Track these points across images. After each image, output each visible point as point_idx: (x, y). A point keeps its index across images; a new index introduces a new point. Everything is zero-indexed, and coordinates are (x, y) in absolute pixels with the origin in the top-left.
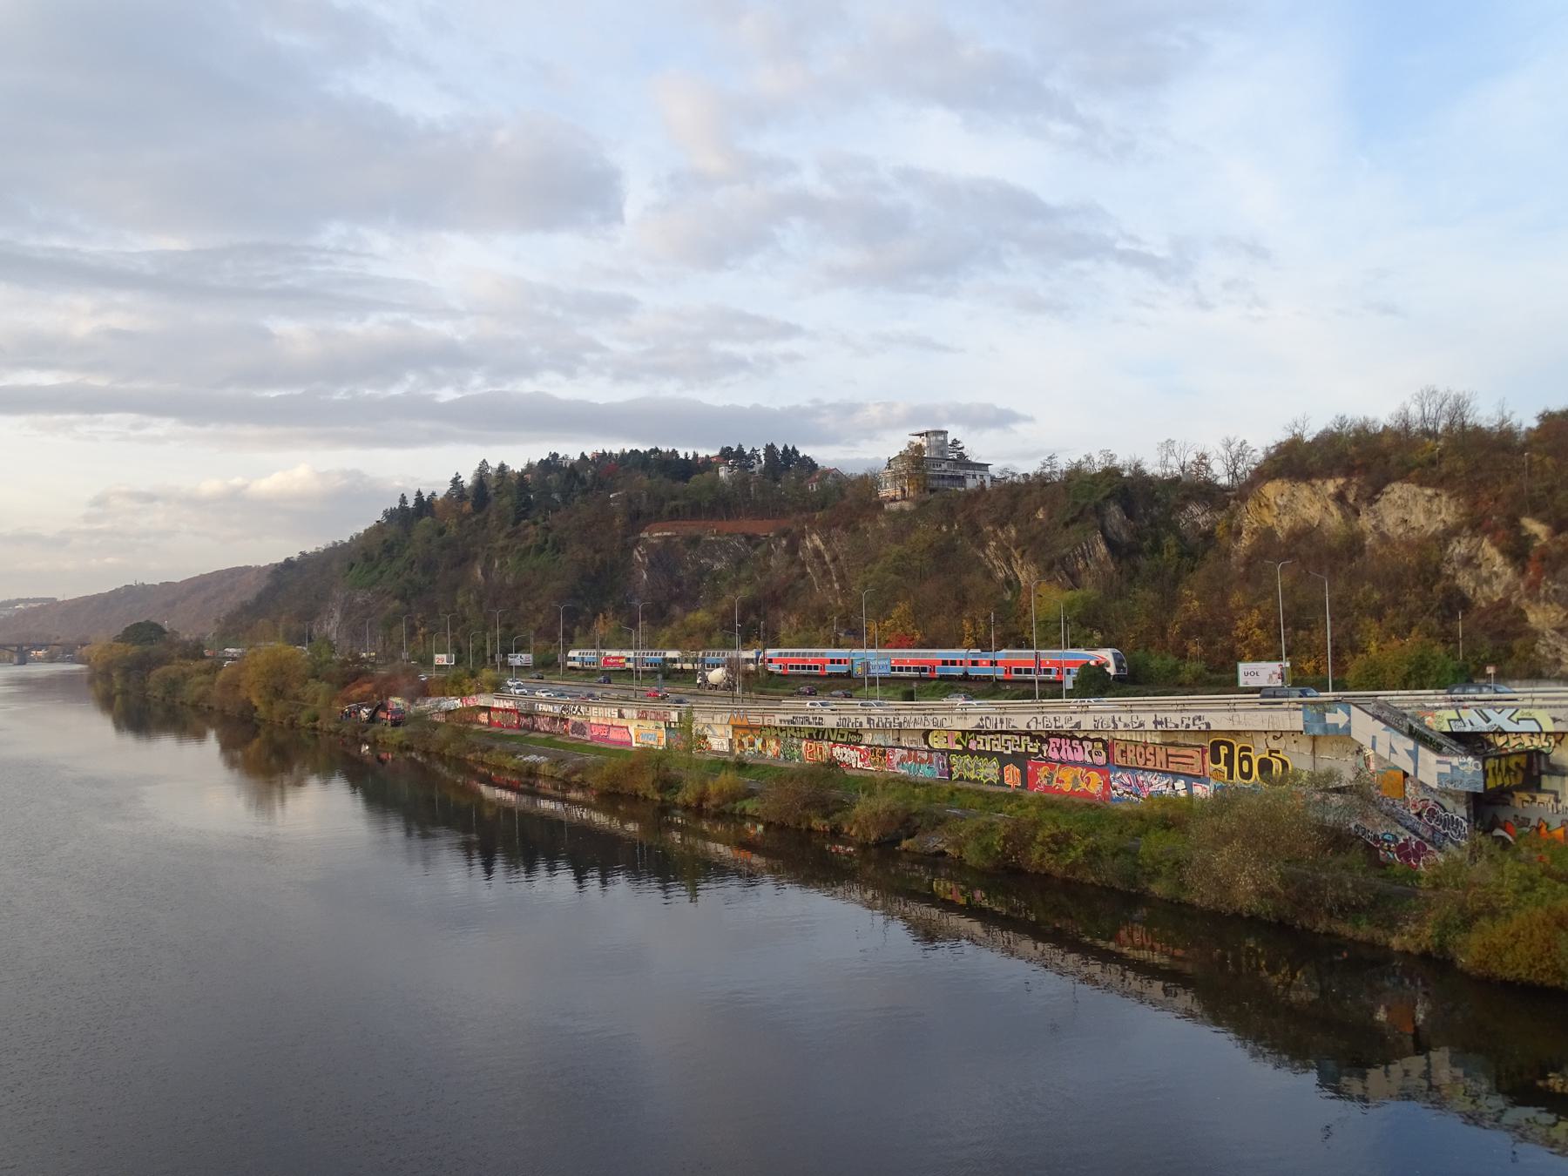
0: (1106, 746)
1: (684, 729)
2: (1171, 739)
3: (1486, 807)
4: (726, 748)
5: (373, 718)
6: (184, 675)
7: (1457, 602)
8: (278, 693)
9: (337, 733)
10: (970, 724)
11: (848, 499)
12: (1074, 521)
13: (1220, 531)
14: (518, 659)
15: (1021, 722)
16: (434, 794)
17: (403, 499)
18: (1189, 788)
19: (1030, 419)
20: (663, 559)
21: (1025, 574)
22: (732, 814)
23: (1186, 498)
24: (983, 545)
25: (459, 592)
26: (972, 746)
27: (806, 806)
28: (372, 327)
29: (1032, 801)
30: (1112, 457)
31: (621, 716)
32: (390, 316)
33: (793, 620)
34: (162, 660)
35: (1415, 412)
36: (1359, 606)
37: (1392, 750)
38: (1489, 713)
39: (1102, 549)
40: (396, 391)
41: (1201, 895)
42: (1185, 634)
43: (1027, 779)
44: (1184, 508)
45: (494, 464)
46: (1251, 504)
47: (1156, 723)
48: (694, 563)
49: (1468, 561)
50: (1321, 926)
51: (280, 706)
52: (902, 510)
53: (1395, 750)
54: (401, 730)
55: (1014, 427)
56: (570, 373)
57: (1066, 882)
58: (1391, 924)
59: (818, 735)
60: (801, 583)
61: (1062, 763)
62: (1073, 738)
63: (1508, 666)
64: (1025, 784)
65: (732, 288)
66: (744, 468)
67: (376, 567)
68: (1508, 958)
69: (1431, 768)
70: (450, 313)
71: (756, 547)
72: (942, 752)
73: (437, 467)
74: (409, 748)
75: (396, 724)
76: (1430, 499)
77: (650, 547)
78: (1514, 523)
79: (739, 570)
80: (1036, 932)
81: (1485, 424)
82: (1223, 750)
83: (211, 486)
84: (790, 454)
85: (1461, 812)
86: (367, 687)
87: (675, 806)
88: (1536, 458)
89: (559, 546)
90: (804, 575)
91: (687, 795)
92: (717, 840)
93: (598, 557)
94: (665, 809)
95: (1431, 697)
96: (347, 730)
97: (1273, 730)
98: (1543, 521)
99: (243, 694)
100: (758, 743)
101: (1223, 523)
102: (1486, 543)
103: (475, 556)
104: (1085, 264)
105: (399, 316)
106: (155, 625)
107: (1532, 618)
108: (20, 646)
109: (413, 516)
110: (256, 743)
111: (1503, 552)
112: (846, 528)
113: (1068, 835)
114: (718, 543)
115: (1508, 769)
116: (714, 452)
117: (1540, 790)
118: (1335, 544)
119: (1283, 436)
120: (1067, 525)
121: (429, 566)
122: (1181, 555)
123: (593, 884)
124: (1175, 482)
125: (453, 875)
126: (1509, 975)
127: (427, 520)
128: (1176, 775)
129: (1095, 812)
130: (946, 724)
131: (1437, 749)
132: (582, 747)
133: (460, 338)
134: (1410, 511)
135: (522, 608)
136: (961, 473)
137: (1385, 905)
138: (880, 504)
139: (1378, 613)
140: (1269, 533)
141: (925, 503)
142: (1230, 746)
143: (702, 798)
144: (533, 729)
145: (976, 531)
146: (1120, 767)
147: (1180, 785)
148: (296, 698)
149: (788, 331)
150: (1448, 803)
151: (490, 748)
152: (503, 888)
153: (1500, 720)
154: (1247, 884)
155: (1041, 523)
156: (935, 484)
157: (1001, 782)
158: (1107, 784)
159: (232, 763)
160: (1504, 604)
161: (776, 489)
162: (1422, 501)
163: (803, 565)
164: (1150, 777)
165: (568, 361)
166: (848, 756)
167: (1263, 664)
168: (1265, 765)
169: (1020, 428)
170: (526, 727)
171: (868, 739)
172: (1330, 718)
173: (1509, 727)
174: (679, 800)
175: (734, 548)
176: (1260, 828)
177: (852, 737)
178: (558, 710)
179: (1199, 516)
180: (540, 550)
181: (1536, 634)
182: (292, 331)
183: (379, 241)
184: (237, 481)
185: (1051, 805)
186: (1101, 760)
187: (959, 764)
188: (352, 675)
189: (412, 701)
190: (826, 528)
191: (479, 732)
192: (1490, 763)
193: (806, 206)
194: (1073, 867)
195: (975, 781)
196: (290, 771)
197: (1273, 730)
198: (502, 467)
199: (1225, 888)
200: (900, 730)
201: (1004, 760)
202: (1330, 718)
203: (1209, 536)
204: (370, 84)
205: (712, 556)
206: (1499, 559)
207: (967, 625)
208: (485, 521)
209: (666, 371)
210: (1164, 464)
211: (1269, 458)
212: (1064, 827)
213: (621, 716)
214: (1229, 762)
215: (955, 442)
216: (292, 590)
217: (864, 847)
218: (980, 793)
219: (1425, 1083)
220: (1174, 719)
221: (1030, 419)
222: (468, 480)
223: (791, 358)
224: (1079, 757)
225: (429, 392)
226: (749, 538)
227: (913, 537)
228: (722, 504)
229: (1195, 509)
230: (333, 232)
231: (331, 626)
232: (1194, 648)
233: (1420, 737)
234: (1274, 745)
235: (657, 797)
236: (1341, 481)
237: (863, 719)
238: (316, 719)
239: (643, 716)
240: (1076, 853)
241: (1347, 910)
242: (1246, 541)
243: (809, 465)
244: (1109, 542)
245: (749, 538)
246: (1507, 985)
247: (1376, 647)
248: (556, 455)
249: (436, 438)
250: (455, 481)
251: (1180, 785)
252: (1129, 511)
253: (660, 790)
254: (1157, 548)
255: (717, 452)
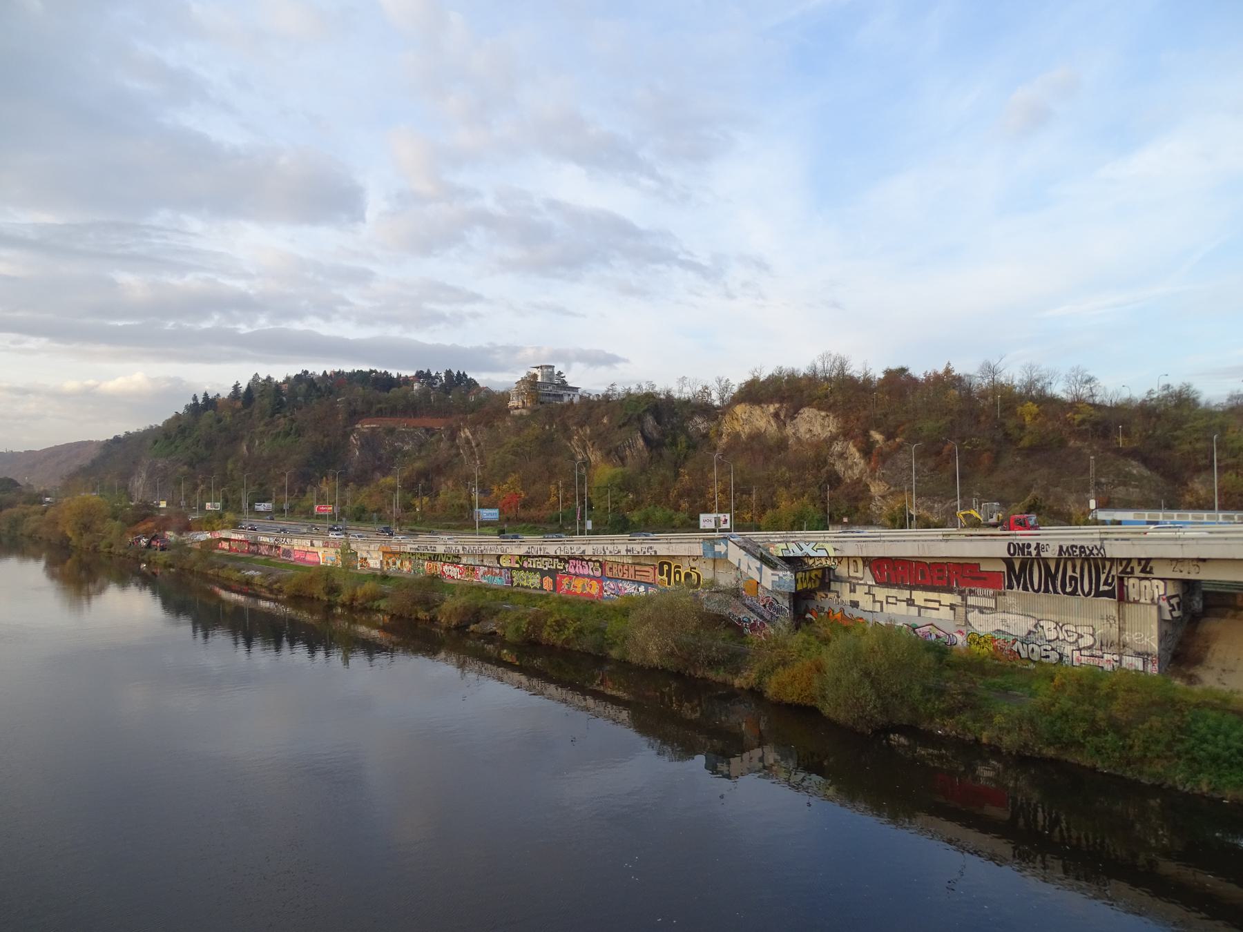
0: (601, 565)
1: (349, 555)
2: (638, 560)
3: (800, 600)
4: (378, 566)
5: (149, 546)
6: (25, 516)
7: (835, 480)
8: (86, 528)
9: (124, 555)
10: (523, 550)
11: (485, 407)
12: (624, 425)
13: (712, 434)
14: (262, 507)
15: (552, 549)
16: (194, 594)
17: (195, 398)
18: (646, 590)
19: (626, 361)
20: (369, 442)
21: (594, 456)
22: (371, 609)
23: (693, 413)
24: (570, 439)
25: (230, 461)
26: (525, 565)
27: (414, 604)
28: (191, 281)
29: (555, 600)
30: (653, 386)
31: (312, 545)
32: (202, 275)
33: (450, 483)
34: (11, 505)
36: (778, 481)
37: (749, 568)
38: (802, 545)
39: (641, 443)
40: (206, 325)
41: (635, 658)
42: (680, 496)
43: (556, 585)
44: (691, 419)
45: (263, 376)
46: (727, 418)
47: (627, 551)
49: (842, 455)
50: (699, 674)
51: (87, 537)
52: (521, 415)
53: (751, 567)
54: (166, 554)
55: (617, 365)
56: (327, 319)
57: (564, 649)
58: (737, 672)
59: (434, 558)
60: (456, 460)
61: (577, 575)
62: (583, 560)
63: (855, 518)
64: (555, 589)
65: (441, 268)
66: (430, 385)
67: (172, 443)
68: (789, 689)
69: (769, 578)
70: (247, 276)
72: (508, 568)
73: (223, 377)
74: (171, 566)
75: (163, 549)
76: (824, 418)
77: (362, 434)
78: (866, 433)
79: (420, 451)
80: (561, 683)
81: (856, 375)
82: (666, 567)
83: (71, 385)
84: (461, 377)
85: (785, 604)
86: (150, 525)
87: (336, 604)
88: (880, 396)
89: (299, 433)
90: (458, 454)
91: (344, 597)
94: (330, 606)
95: (774, 536)
96: (131, 554)
97: (726, 559)
98: (881, 433)
99: (60, 529)
100: (398, 563)
101: (714, 429)
102: (851, 445)
103: (242, 438)
104: (661, 267)
105: (209, 275)
106: (11, 480)
107: (872, 489)
109: (205, 407)
110: (69, 562)
111: (859, 450)
112: (486, 425)
113: (564, 621)
115: (810, 578)
116: (411, 373)
117: (830, 591)
118: (771, 443)
119: (749, 378)
120: (620, 427)
121: (210, 444)
122: (688, 447)
123: (320, 655)
124: (687, 402)
125: (222, 650)
126: (788, 700)
127: (211, 412)
128: (640, 583)
129: (590, 603)
130: (509, 551)
131: (773, 566)
132: (289, 565)
133: (251, 292)
134: (813, 425)
135: (272, 472)
136: (561, 392)
137: (734, 661)
138: (508, 411)
139: (787, 485)
140: (738, 435)
141: (536, 411)
142: (670, 565)
143: (353, 599)
144: (257, 553)
145: (565, 429)
146: (609, 578)
147: (642, 589)
148: (98, 531)
149: (476, 298)
150: (780, 599)
151: (224, 566)
152: (261, 656)
153: (808, 550)
154: (649, 647)
155: (605, 425)
156: (543, 399)
157: (541, 588)
158: (602, 588)
159: (52, 576)
160: (859, 481)
161: (449, 398)
162: (819, 419)
163: (458, 448)
164: (625, 584)
165: (326, 310)
166: (452, 571)
168: (688, 576)
169: (620, 366)
170: (253, 552)
171: (464, 560)
172: (717, 548)
173: (812, 554)
174: (339, 600)
176: (664, 614)
177: (454, 559)
178: (272, 541)
179: (700, 424)
180: (288, 434)
181: (872, 498)
182: (132, 282)
183: (194, 224)
184: (91, 382)
185: (567, 602)
186: (598, 574)
187: (519, 577)
188: (146, 512)
189: (181, 534)
190: (473, 424)
191: (221, 556)
192: (800, 575)
193: (487, 220)
194: (567, 641)
195: (527, 587)
196: (95, 582)
197: (726, 559)
198: (269, 378)
199: (644, 651)
201: (543, 573)
202: (717, 548)
203: (705, 436)
204: (192, 119)
206: (857, 455)
207: (553, 488)
208: (251, 414)
209: (391, 320)
210: (681, 391)
211: (741, 391)
212: (564, 615)
213: (312, 545)
214: (669, 576)
215: (560, 373)
216: (120, 454)
217: (448, 629)
218: (526, 594)
219: (761, 765)
220: (638, 548)
221: (626, 361)
222: (244, 386)
223: (475, 315)
224: (586, 571)
225: (230, 326)
226: (427, 430)
227: (526, 432)
228: (412, 408)
229: (698, 420)
230: (162, 217)
231: (139, 484)
232: (684, 505)
233: (766, 560)
234: (693, 565)
235: (325, 598)
236: (777, 405)
237: (460, 548)
238: (111, 546)
239: (326, 545)
240: (569, 632)
241: (713, 664)
242: (725, 439)
243: (472, 384)
244: (645, 438)
245: (427, 430)
246: (789, 706)
247: (786, 506)
248: (306, 372)
249: (234, 358)
250: (236, 387)
251: (642, 589)
252: (658, 419)
253: (328, 593)
254: (674, 443)
255: (413, 373)
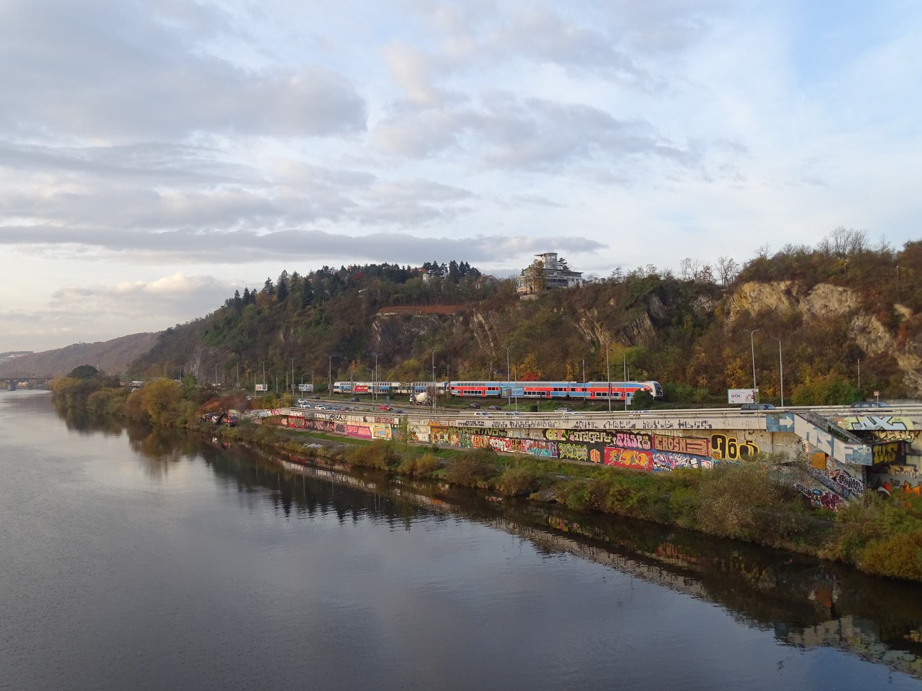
0: (650, 438)
1: (402, 428)
2: (689, 434)
3: (874, 474)
4: (427, 439)
5: (219, 422)
6: (108, 397)
7: (857, 354)
8: (164, 407)
9: (198, 431)
10: (571, 425)
11: (498, 293)
12: (631, 306)
13: (717, 312)
14: (304, 387)
15: (600, 424)
16: (255, 467)
17: (237, 293)
18: (699, 463)
19: (606, 246)
20: (390, 329)
21: (603, 337)
22: (430, 478)
23: (698, 293)
24: (578, 320)
25: (270, 348)
26: (572, 438)
27: (474, 473)
28: (219, 192)
29: (607, 471)
30: (654, 269)
31: (365, 421)
32: (229, 186)
33: (466, 364)
34: (95, 388)
35: (832, 242)
36: (799, 356)
37: (819, 441)
38: (876, 419)
39: (648, 323)
40: (233, 229)
41: (706, 526)
42: (697, 373)
43: (604, 458)
44: (696, 298)
45: (290, 273)
46: (736, 296)
47: (680, 425)
48: (408, 331)
49: (863, 330)
50: (777, 544)
51: (165, 415)
52: (530, 300)
53: (820, 440)
54: (236, 429)
55: (596, 251)
56: (335, 219)
57: (627, 518)
58: (818, 543)
59: (481, 432)
60: (471, 343)
61: (625, 448)
62: (631, 433)
63: (887, 392)
64: (603, 461)
65: (430, 169)
66: (437, 275)
67: (221, 333)
68: (887, 563)
69: (841, 451)
70: (264, 184)
71: (444, 321)
72: (554, 442)
73: (257, 274)
74: (240, 440)
75: (233, 425)
76: (841, 293)
77: (382, 322)
78: (890, 307)
79: (434, 335)
80: (609, 548)
81: (873, 249)
82: (719, 441)
83: (124, 285)
84: (465, 267)
85: (859, 477)
86: (216, 404)
87: (397, 474)
88: (903, 269)
89: (329, 321)
90: (473, 338)
91: (404, 467)
92: (421, 494)
93: (352, 327)
94: (391, 476)
95: (841, 410)
96: (204, 429)
97: (749, 429)
98: (907, 306)
99: (143, 408)
100: (446, 437)
101: (719, 308)
102: (874, 319)
103: (280, 327)
104: (638, 155)
105: (235, 186)
106: (91, 367)
107: (901, 363)
108: (12, 380)
109: (243, 303)
110: (151, 436)
111: (884, 324)
112: (497, 310)
113: (628, 491)
114: (422, 319)
115: (887, 452)
116: (420, 266)
117: (905, 464)
118: (785, 319)
119: (755, 256)
120: (627, 308)
121: (252, 333)
122: (695, 326)
123: (349, 519)
124: (691, 283)
125: (266, 514)
126: (887, 573)
127: (251, 305)
128: (692, 456)
129: (644, 477)
130: (557, 425)
131: (845, 440)
132: (342, 439)
133: (270, 198)
134: (829, 300)
135: (307, 357)
136: (565, 278)
137: (814, 532)
138: (517, 296)
139: (810, 360)
140: (746, 313)
141: (544, 296)
142: (724, 439)
143: (413, 469)
144: (313, 429)
145: (574, 312)
146: (658, 451)
147: (694, 461)
148: (174, 410)
149: (464, 194)
150: (852, 472)
151: (288, 440)
152: (296, 521)
153: (882, 423)
154: (733, 519)
155: (612, 307)
156: (550, 284)
157: (589, 460)
158: (651, 461)
159: (136, 448)
160: (885, 355)
161: (456, 287)
162: (836, 295)
163: (472, 332)
164: (676, 457)
165: (334, 212)
166: (499, 444)
167: (743, 390)
168: (744, 450)
169: (600, 251)
170: (309, 427)
171: (510, 434)
172: (782, 422)
173: (887, 427)
174: (399, 470)
175: (432, 322)
176: (741, 487)
177: (501, 433)
178: (328, 417)
179: (705, 303)
180: (318, 323)
181: (903, 373)
182: (172, 194)
183: (223, 141)
184: (140, 283)
185: (618, 473)
186: (648, 446)
187: (564, 449)
188: (207, 397)
189: (242, 412)
190: (485, 310)
191: (282, 430)
192: (876, 449)
193: (474, 121)
194: (631, 510)
195: (574, 459)
196: (171, 453)
197: (749, 429)
198: (295, 275)
199: (721, 522)
200: (529, 429)
201: (590, 446)
202: (782, 422)
203: (711, 315)
204: (218, 49)
205: (419, 327)
206: (881, 329)
207: (569, 367)
208: (285, 306)
209: (391, 218)
210: (685, 273)
211: (746, 269)
212: (625, 486)
213: (365, 421)
214: (723, 448)
215: (562, 260)
216: (171, 346)
217: (508, 498)
218: (576, 466)
219: (838, 637)
220: (691, 422)
221: (606, 246)
222: (275, 282)
223: (465, 210)
224: (634, 445)
225: (253, 230)
226: (440, 316)
227: (537, 316)
228: (425, 296)
229: (703, 299)
230: (196, 137)
231: (195, 368)
232: (702, 381)
233: (835, 433)
234: (749, 438)
235: (386, 468)
236: (788, 283)
237: (508, 423)
238: (186, 423)
239: (378, 421)
240: (633, 501)
241: (792, 534)
242: (733, 318)
243: (476, 273)
244: (652, 319)
245: (440, 316)
246: (886, 579)
247: (809, 380)
248: (327, 267)
249: (256, 257)
250: (268, 283)
251: (694, 461)
252: (664, 300)
253: (388, 464)
254: (680, 322)
255: (422, 266)
